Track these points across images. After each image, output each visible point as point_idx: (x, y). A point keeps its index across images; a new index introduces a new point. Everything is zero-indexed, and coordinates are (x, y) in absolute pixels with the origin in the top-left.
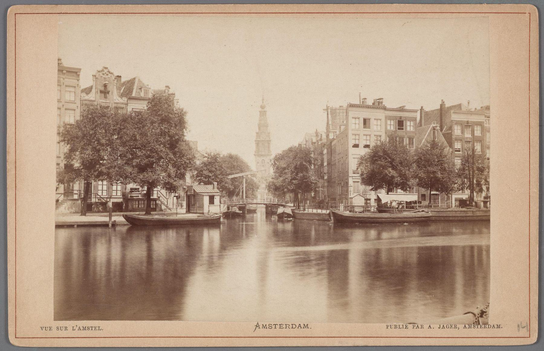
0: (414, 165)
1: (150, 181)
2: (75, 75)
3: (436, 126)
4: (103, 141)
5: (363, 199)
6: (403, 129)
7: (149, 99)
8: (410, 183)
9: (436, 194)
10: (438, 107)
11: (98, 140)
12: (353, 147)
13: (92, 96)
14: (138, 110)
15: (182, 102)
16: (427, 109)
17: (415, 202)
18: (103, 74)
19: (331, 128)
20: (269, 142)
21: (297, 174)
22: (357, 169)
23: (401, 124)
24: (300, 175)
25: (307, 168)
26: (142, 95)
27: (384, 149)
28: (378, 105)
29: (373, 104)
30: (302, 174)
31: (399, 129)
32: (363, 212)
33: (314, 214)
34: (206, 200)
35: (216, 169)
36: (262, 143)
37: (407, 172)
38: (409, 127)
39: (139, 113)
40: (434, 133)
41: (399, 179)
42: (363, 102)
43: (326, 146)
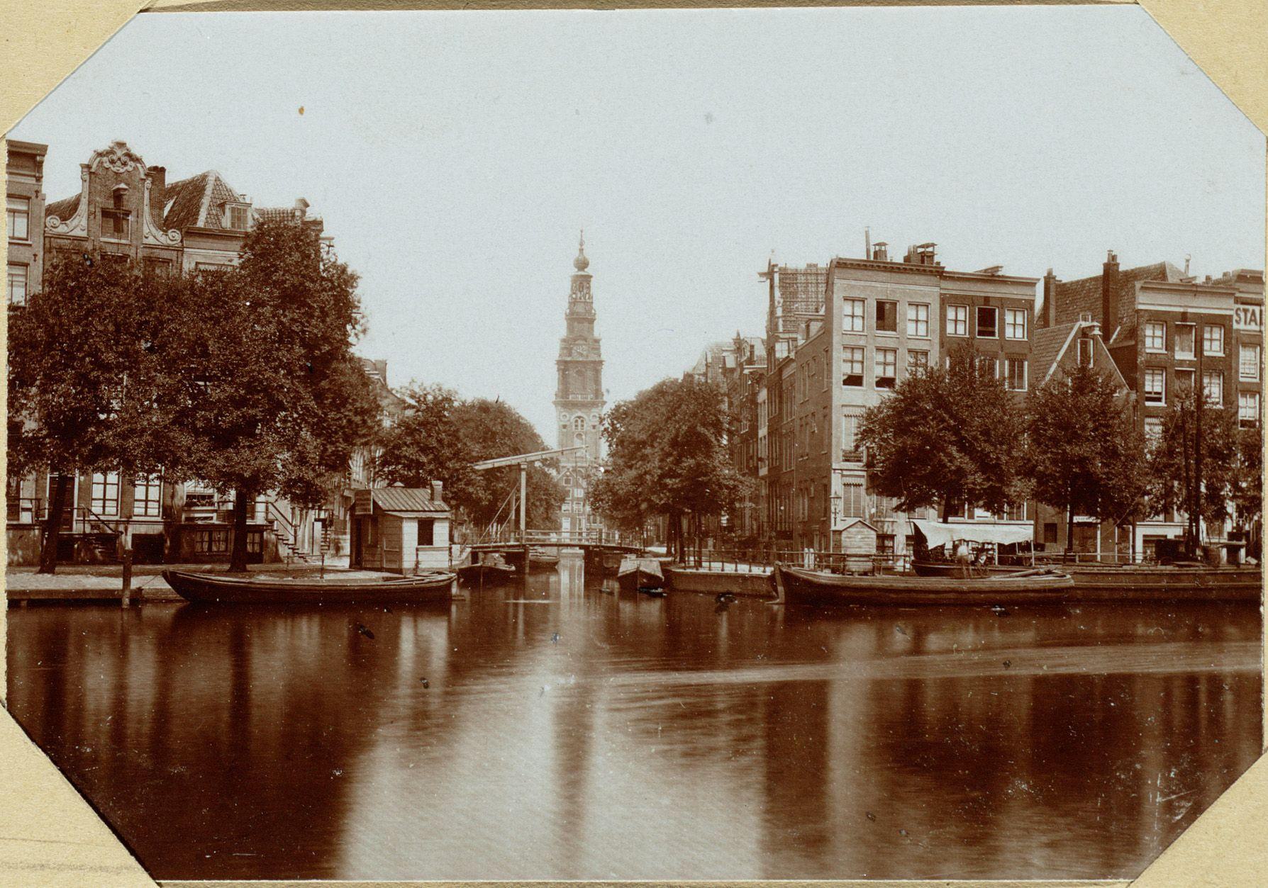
0: (1025, 440)
1: (247, 475)
2: (30, 164)
3: (1092, 328)
4: (110, 357)
5: (873, 535)
6: (993, 334)
7: (247, 235)
8: (1012, 491)
9: (1089, 525)
10: (1098, 271)
11: (95, 353)
12: (846, 382)
13: (78, 226)
14: (212, 268)
15: (343, 246)
16: (1066, 275)
17: (1025, 547)
18: (112, 162)
19: (781, 329)
20: (597, 365)
21: (678, 462)
22: (857, 447)
23: (986, 319)
24: (689, 462)
25: (708, 444)
26: (226, 222)
27: (936, 391)
29: (907, 259)
30: (692, 462)
32: (872, 572)
34: (410, 531)
35: (440, 441)
36: (578, 368)
37: (1004, 458)
38: (1013, 328)
39: (218, 275)
40: (1084, 344)
41: (979, 478)
42: (876, 253)
43: (765, 382)
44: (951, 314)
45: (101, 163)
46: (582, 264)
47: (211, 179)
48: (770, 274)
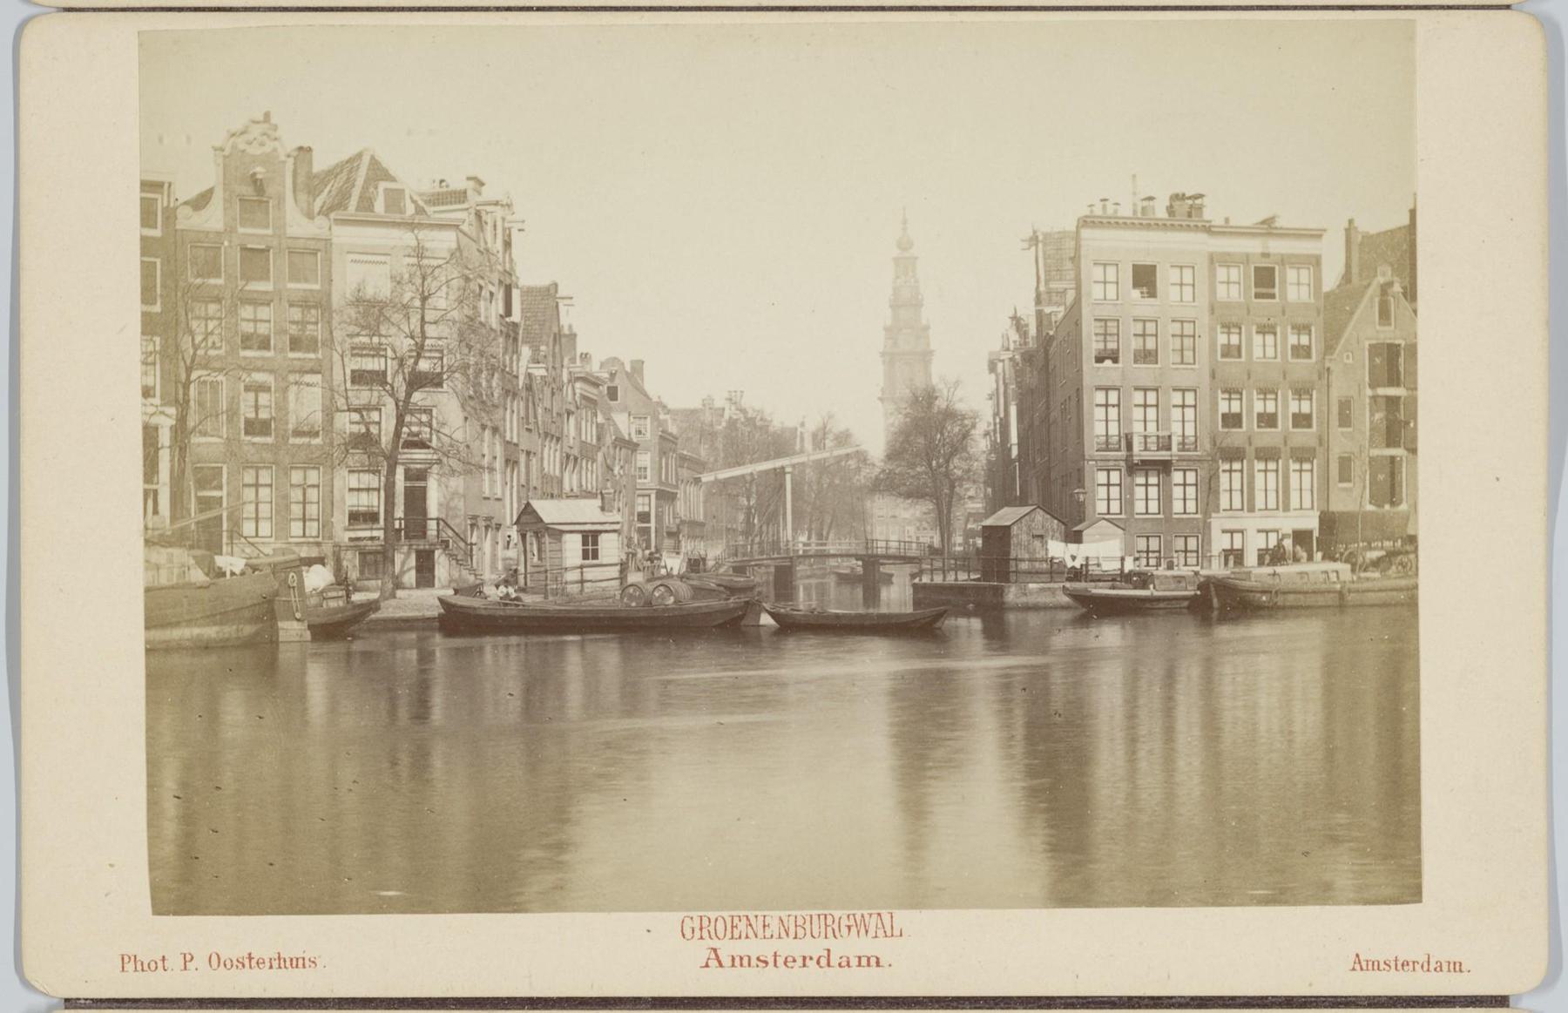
6: (1273, 296)
18: (250, 143)
23: (1265, 279)
28: (1186, 211)
31: (1257, 296)
33: (951, 588)
42: (1143, 208)
44: (1222, 273)
45: (234, 147)
46: (905, 245)
47: (366, 160)
48: (1034, 240)
